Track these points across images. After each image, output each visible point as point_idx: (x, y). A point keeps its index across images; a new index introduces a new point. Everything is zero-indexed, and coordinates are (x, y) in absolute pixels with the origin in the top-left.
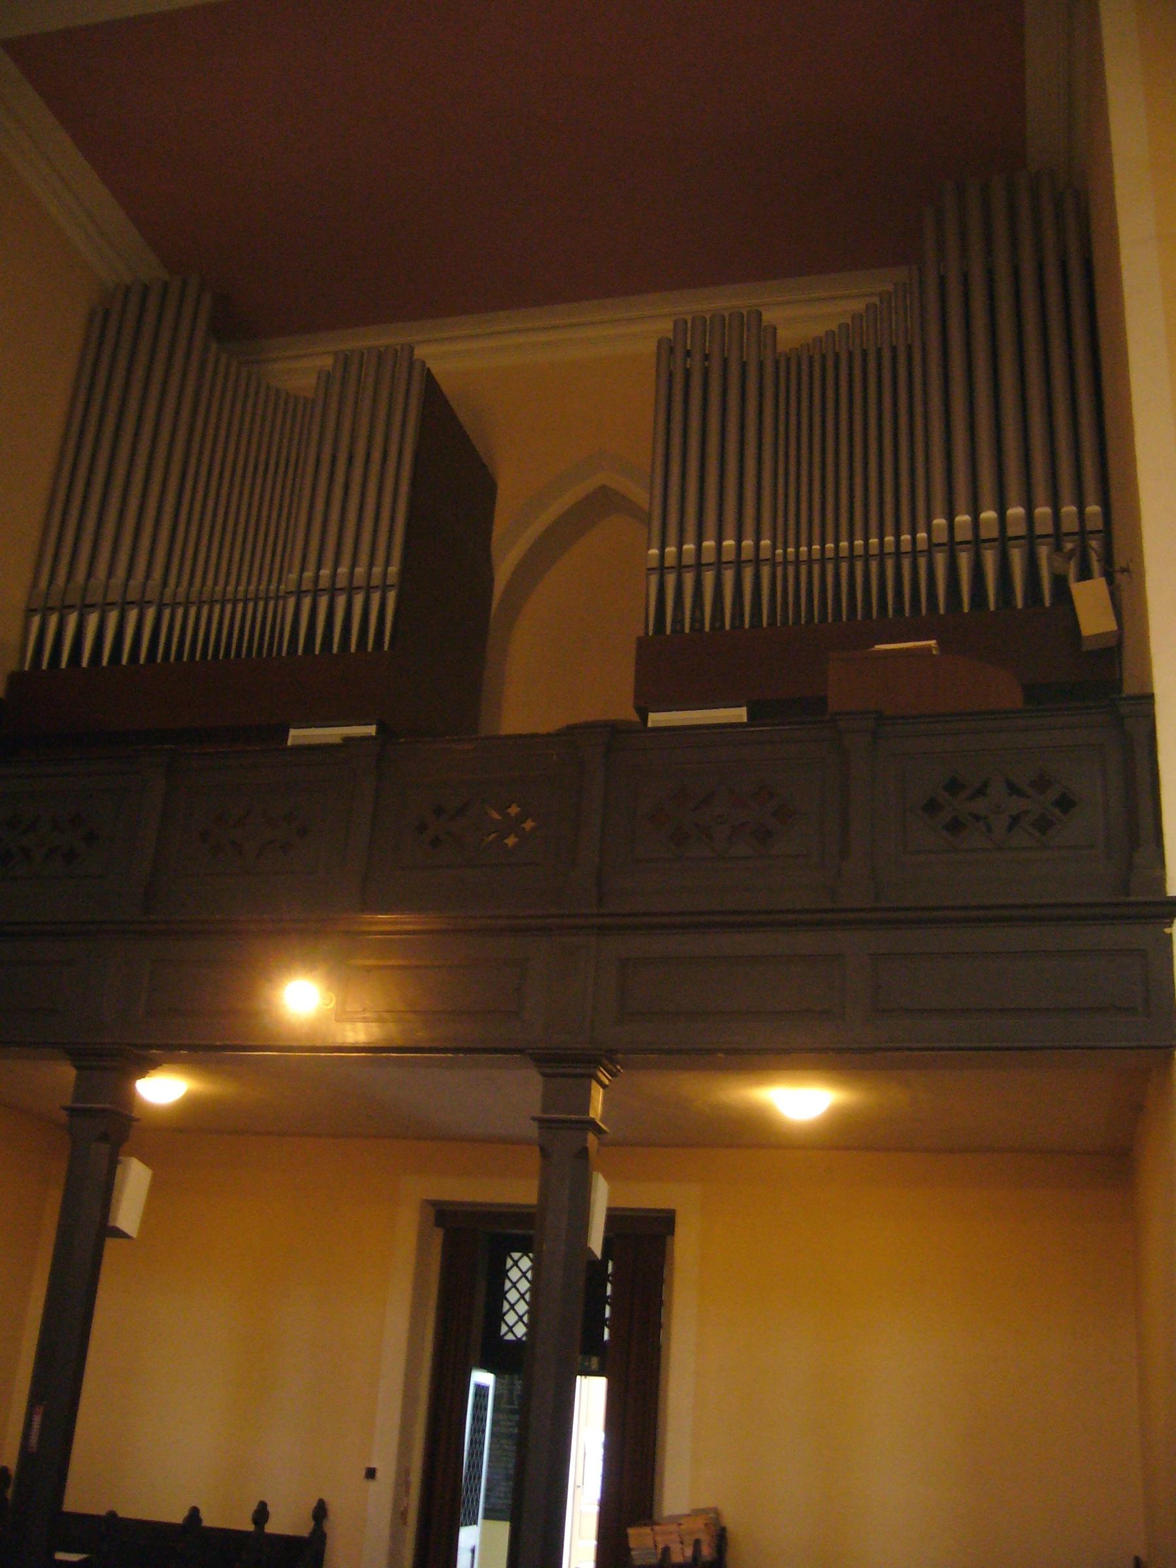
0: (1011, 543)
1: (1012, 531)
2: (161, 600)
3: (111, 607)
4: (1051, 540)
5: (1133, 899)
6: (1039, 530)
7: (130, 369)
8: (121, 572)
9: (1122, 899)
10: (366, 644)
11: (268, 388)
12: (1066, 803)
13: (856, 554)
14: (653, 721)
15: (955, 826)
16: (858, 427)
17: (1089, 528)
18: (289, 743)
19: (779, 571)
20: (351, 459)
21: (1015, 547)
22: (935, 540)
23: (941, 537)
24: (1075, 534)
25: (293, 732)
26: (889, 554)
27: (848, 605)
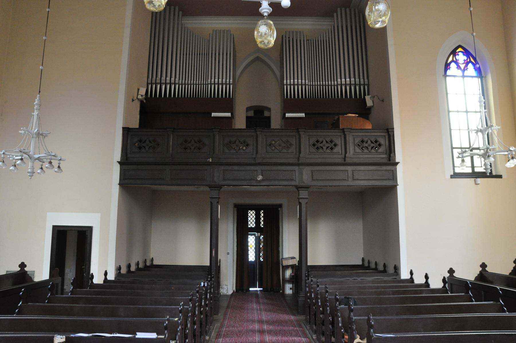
0: (343, 85)
1: (352, 83)
2: (201, 84)
3: (163, 84)
4: (340, 85)
5: (300, 162)
6: (365, 83)
7: (342, 17)
8: (155, 77)
9: (298, 162)
10: (291, 96)
11: (231, 35)
12: (335, 145)
13: (303, 84)
14: (213, 115)
15: (318, 148)
16: (317, 54)
17: (342, 83)
18: (212, 116)
19: (181, 86)
20: (219, 54)
21: (343, 86)
22: (208, 83)
23: (339, 83)
24: (358, 84)
25: (213, 114)
26: (292, 84)
27: (178, 94)
